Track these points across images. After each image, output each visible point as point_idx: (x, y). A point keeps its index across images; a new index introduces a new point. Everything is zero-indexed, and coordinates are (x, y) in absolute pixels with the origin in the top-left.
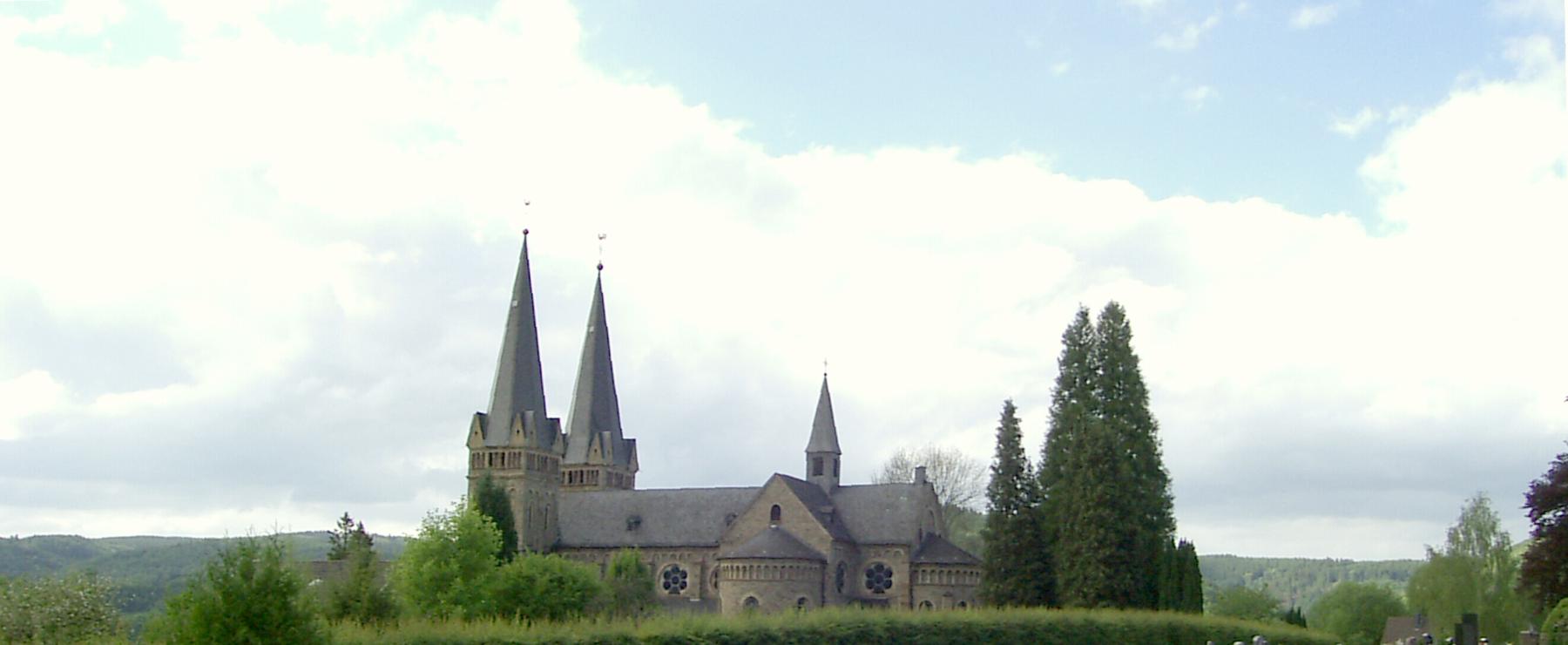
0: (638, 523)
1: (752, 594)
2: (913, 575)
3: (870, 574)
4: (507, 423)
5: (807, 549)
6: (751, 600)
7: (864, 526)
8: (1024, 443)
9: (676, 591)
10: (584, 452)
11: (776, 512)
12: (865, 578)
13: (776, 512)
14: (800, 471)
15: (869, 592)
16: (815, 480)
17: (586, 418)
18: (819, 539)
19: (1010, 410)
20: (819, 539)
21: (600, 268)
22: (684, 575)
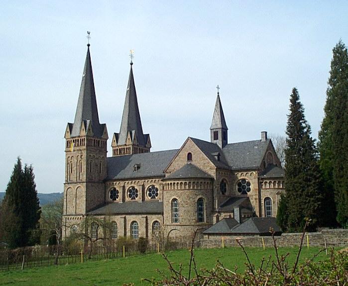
0: (139, 167)
1: (175, 197)
2: (260, 185)
3: (239, 184)
4: (79, 126)
5: (205, 173)
6: (175, 200)
7: (233, 161)
8: (307, 117)
9: (154, 197)
10: (124, 141)
11: (190, 156)
12: (237, 187)
13: (190, 156)
14: (207, 137)
15: (240, 194)
16: (215, 142)
17: (126, 125)
18: (209, 168)
19: (295, 91)
20: (209, 168)
21: (132, 64)
22: (157, 190)
